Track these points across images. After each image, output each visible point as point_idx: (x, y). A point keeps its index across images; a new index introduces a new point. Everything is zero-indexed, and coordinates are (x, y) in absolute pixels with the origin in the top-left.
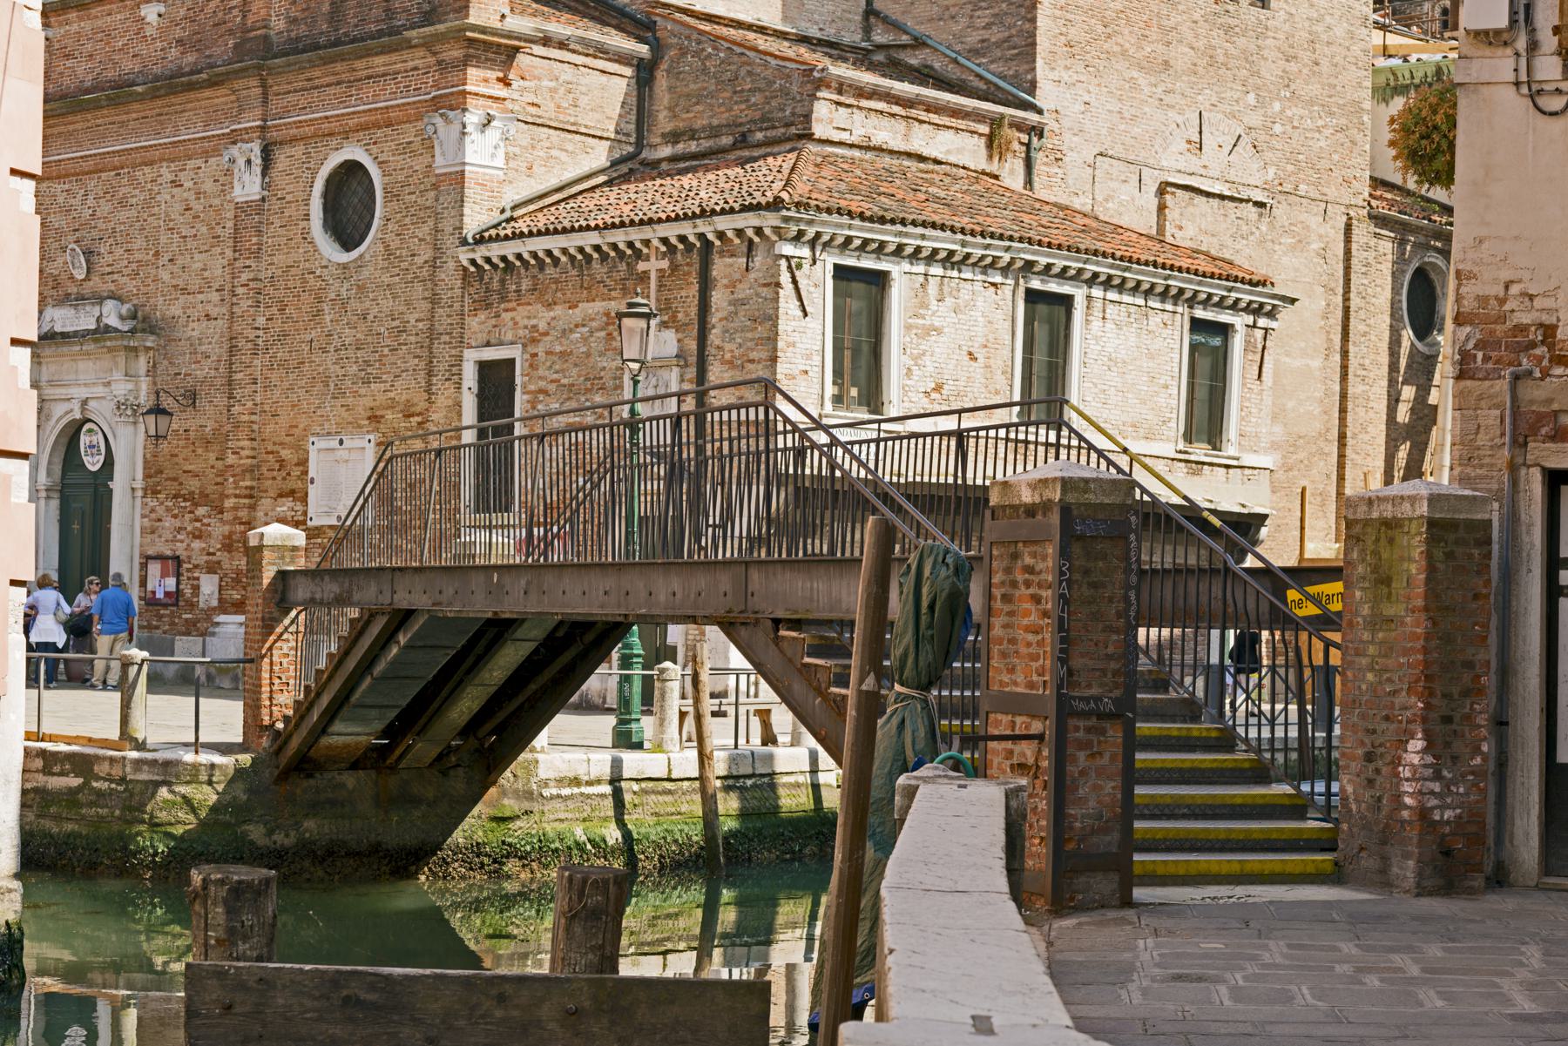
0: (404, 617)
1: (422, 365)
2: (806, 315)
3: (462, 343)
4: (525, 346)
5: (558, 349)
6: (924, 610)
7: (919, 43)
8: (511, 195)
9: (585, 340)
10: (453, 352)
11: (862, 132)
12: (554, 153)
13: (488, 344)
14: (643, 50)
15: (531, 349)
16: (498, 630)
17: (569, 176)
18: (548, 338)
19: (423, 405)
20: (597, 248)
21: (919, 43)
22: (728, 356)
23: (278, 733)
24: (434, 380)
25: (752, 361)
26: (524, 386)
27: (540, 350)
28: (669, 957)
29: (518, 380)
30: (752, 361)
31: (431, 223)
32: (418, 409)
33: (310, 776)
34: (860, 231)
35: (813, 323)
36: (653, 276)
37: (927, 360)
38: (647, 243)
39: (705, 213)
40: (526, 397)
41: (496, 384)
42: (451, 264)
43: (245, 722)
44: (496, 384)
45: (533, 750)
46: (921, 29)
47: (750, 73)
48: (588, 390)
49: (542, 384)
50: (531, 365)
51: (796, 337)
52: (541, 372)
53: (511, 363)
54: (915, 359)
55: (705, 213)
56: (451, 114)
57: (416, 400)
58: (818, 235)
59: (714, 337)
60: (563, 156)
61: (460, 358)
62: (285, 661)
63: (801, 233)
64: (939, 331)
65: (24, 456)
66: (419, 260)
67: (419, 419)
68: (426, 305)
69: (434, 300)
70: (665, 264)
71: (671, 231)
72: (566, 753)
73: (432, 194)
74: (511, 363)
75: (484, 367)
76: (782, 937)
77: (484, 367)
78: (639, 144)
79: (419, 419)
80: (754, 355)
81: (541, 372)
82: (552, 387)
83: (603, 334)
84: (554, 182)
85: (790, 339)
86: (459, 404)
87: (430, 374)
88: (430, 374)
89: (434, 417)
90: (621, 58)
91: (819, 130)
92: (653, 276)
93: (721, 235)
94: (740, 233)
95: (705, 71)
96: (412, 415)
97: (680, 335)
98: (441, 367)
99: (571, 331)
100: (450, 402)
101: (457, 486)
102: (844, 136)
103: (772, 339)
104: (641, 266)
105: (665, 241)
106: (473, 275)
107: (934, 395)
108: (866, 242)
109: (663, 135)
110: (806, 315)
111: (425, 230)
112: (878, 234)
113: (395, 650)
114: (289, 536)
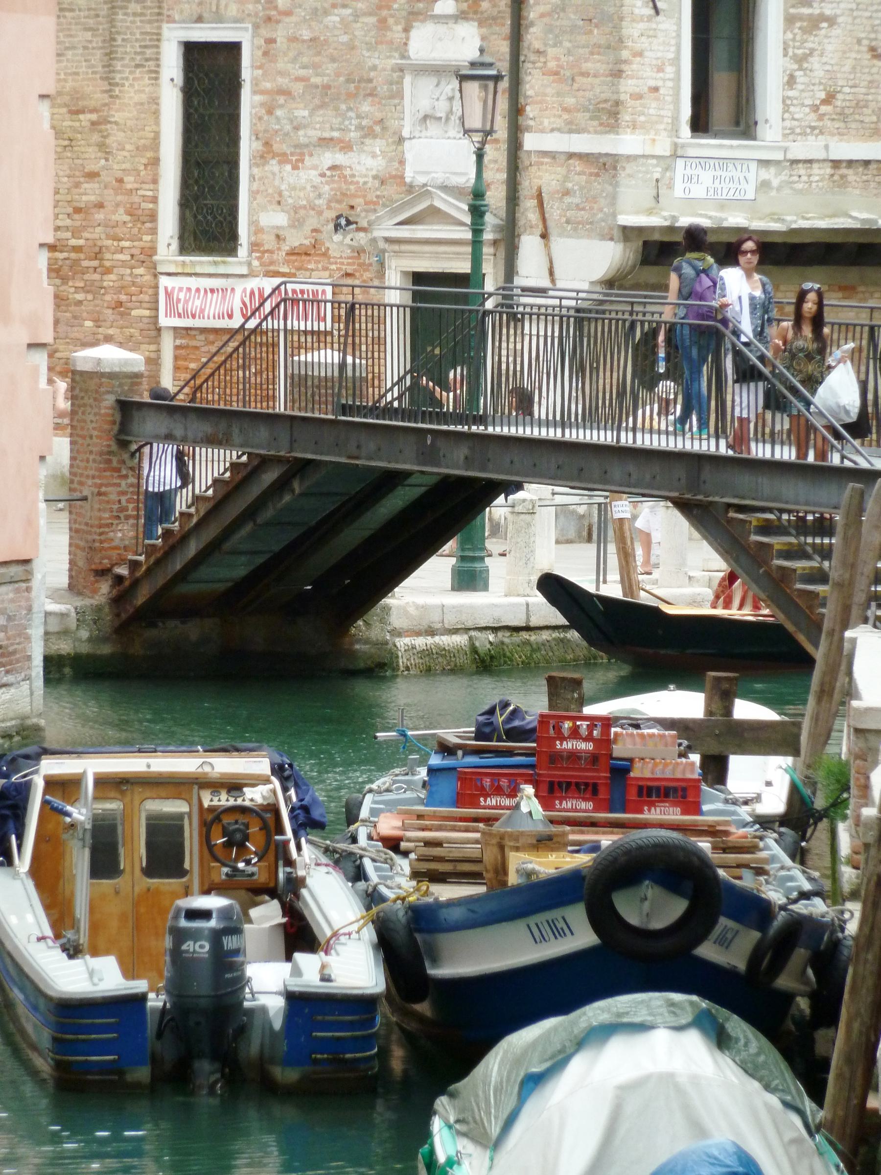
0: (302, 467)
1: (97, 42)
2: (657, 11)
4: (256, 27)
5: (306, 34)
10: (148, 28)
13: (200, 19)
15: (265, 32)
16: (392, 479)
18: (293, 19)
19: (98, 97)
22: (552, 65)
23: (119, 579)
24: (118, 65)
25: (586, 74)
26: (255, 82)
27: (280, 34)
28: (255, 990)
30: (586, 74)
32: (92, 104)
33: (153, 625)
35: (664, 24)
37: (814, 62)
40: (258, 98)
43: (72, 562)
45: (393, 596)
48: (351, 96)
49: (282, 81)
50: (266, 54)
51: (643, 43)
52: (280, 65)
53: (234, 48)
57: (88, 90)
59: (533, 37)
61: (157, 38)
62: (123, 499)
64: (832, 21)
65: (44, 345)
67: (94, 117)
74: (234, 48)
75: (193, 52)
76: (238, 1162)
77: (193, 52)
79: (94, 117)
80: (588, 66)
81: (280, 65)
82: (298, 88)
83: (372, 20)
85: (638, 47)
86: (155, 101)
87: (110, 56)
88: (110, 56)
89: (117, 117)
96: (82, 112)
97: (484, 30)
98: (128, 49)
99: (326, 13)
100: (144, 97)
101: (153, 217)
103: (616, 43)
107: (824, 109)
110: (657, 11)
113: (287, 498)
114: (126, 362)
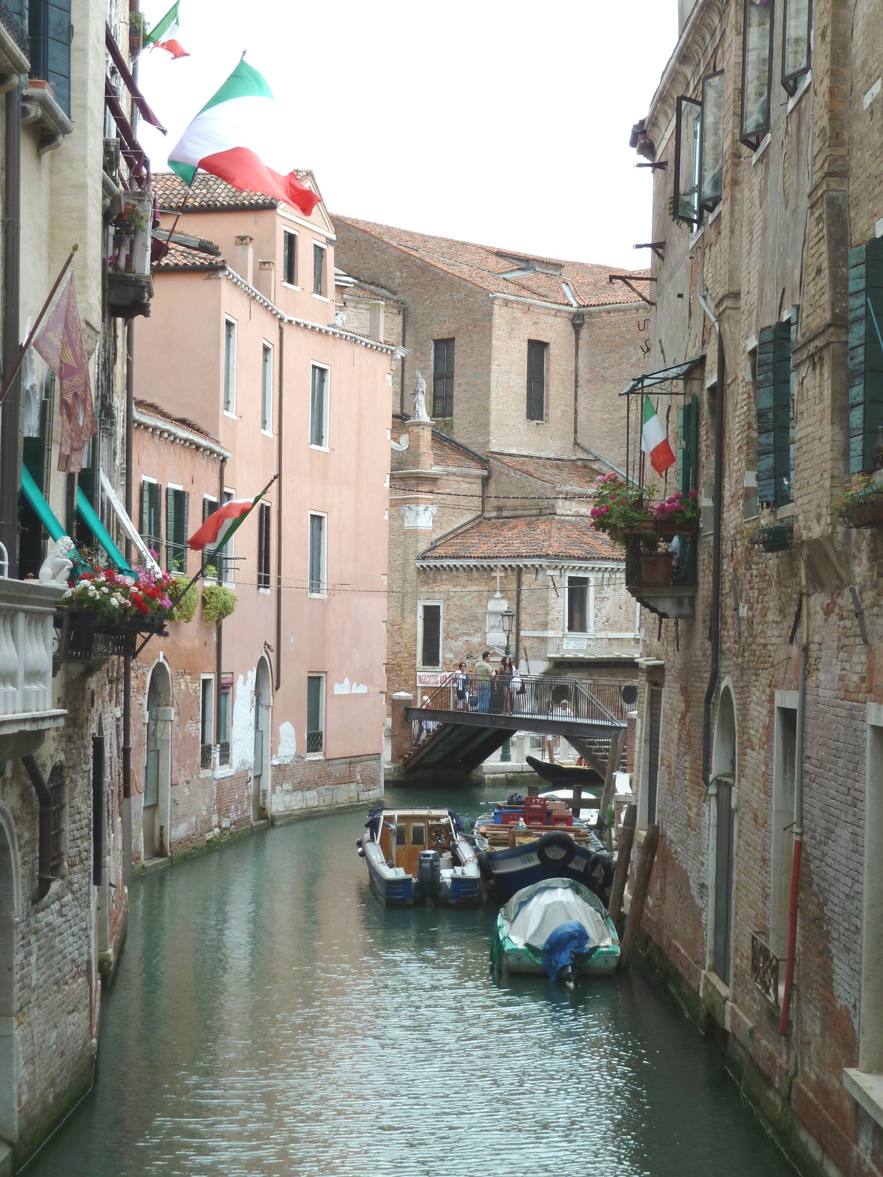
0: (457, 726)
3: (417, 598)
6: (751, 89)
7: (597, 459)
8: (435, 537)
9: (470, 601)
11: (575, 510)
12: (451, 518)
14: (485, 473)
16: (482, 730)
17: (456, 526)
20: (475, 566)
21: (597, 459)
27: (451, 603)
29: (441, 615)
31: (402, 548)
34: (577, 564)
35: (560, 600)
36: (498, 578)
38: (496, 566)
39: (520, 556)
41: (432, 615)
42: (412, 566)
44: (432, 615)
46: (596, 453)
47: (530, 486)
54: (599, 610)
55: (520, 556)
56: (412, 506)
58: (563, 567)
59: (523, 604)
60: (454, 519)
63: (556, 567)
64: (608, 598)
66: (397, 563)
68: (400, 581)
69: (404, 580)
70: (503, 574)
71: (506, 563)
72: (493, 762)
73: (403, 537)
75: (427, 609)
78: (483, 511)
84: (451, 529)
86: (416, 622)
87: (403, 609)
88: (403, 609)
90: (477, 477)
91: (559, 511)
92: (498, 578)
93: (526, 566)
94: (533, 566)
95: (511, 482)
101: (415, 655)
102: (569, 512)
104: (493, 574)
105: (503, 566)
106: (422, 570)
108: (580, 567)
109: (493, 507)
111: (399, 551)
112: (584, 564)
